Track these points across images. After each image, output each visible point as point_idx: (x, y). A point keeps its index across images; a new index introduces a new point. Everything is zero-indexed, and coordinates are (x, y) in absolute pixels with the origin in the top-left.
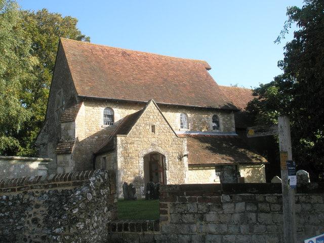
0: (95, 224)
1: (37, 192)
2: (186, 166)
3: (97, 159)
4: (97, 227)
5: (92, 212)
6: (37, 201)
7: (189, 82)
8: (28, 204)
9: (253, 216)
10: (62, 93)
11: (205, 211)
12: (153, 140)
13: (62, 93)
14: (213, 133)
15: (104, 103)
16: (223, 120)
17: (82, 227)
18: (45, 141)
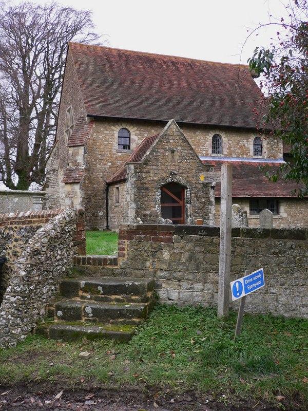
0: (58, 257)
1: (16, 228)
4: (61, 259)
6: (16, 236)
8: (8, 237)
9: (200, 256)
10: (72, 111)
13: (72, 111)
15: (119, 123)
16: (268, 143)
18: (56, 166)
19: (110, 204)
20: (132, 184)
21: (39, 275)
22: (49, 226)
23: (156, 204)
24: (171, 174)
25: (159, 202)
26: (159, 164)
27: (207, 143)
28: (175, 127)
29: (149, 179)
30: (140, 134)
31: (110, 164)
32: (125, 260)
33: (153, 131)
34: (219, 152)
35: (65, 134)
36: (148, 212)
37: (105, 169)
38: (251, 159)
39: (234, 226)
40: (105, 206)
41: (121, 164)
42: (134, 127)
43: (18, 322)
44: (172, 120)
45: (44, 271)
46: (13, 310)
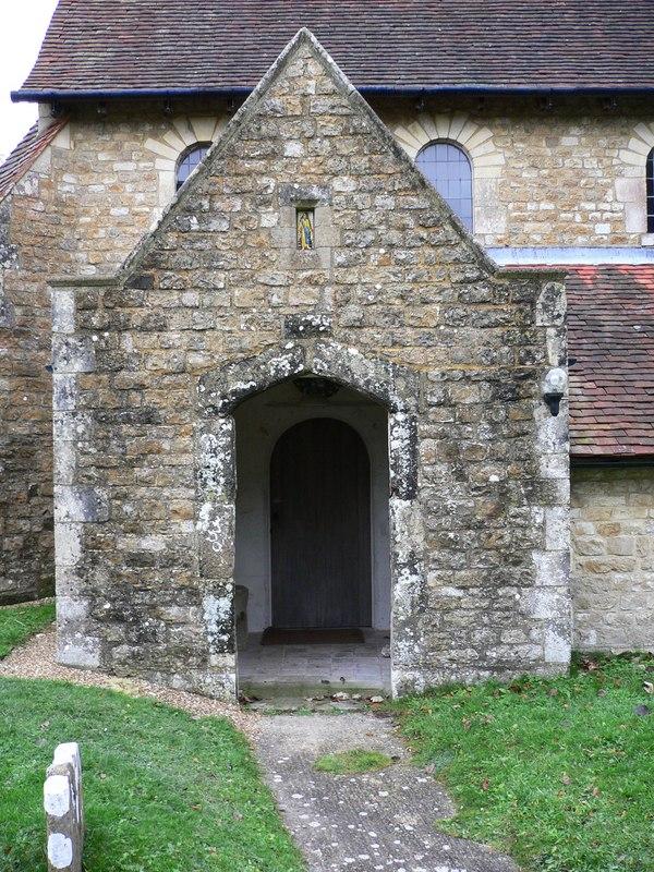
2: (555, 468)
12: (301, 297)
23: (199, 500)
27: (619, 183)
29: (158, 361)
36: (153, 543)
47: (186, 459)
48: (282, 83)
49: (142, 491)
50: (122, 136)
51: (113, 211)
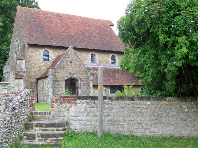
0: (23, 112)
2: (92, 86)
3: (39, 82)
4: (25, 113)
5: (22, 106)
7: (98, 34)
9: (89, 109)
11: (69, 107)
12: (71, 71)
14: (112, 66)
17: (17, 112)
18: (9, 70)
19: (38, 89)
20: (51, 79)
21: (15, 120)
22: (19, 97)
23: (63, 89)
24: (70, 74)
25: (64, 88)
26: (64, 69)
27: (88, 58)
28: (72, 50)
29: (59, 76)
30: (54, 53)
31: (38, 69)
32: (55, 112)
33: (61, 52)
34: (94, 63)
35: (14, 53)
37: (36, 72)
38: (110, 66)
39: (104, 96)
40: (36, 91)
41: (44, 69)
42: (51, 50)
43: (7, 141)
44: (71, 47)
45: (17, 118)
46: (4, 136)
47: (61, 85)
48: (69, 51)
49: (58, 88)
50: (37, 49)
51: (36, 58)
